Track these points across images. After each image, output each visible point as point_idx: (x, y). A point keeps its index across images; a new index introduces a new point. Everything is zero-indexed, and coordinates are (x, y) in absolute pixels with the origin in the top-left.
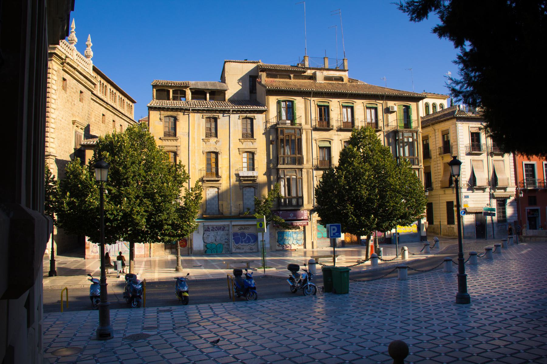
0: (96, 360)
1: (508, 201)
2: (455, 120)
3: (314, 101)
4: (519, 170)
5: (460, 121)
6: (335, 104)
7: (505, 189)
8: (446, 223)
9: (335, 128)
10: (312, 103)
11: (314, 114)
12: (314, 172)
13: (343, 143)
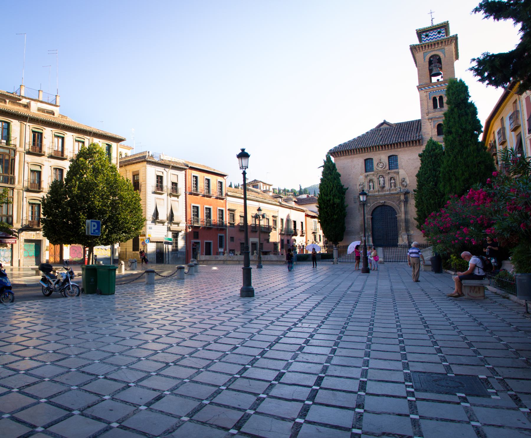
0: (404, 350)
1: (180, 234)
2: (145, 163)
3: (29, 127)
4: (188, 210)
5: (150, 164)
6: (48, 133)
7: (178, 224)
8: (131, 250)
9: (46, 154)
10: (28, 127)
11: (29, 138)
12: (25, 193)
13: (52, 169)
